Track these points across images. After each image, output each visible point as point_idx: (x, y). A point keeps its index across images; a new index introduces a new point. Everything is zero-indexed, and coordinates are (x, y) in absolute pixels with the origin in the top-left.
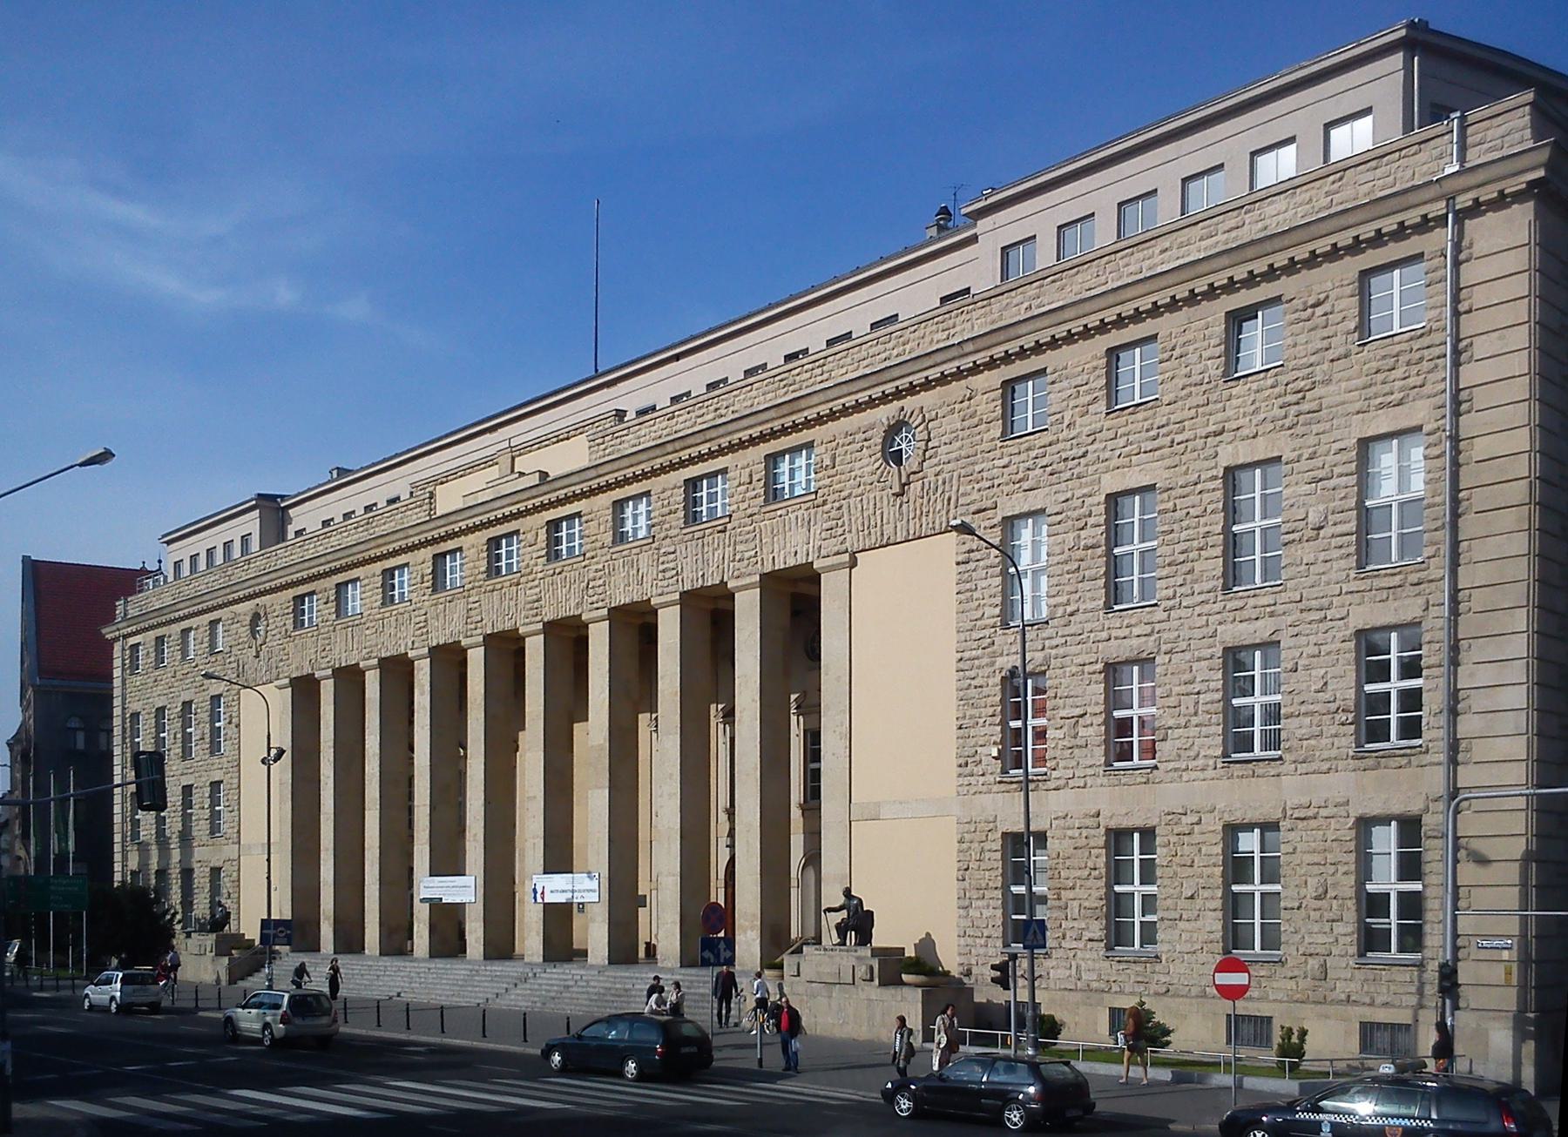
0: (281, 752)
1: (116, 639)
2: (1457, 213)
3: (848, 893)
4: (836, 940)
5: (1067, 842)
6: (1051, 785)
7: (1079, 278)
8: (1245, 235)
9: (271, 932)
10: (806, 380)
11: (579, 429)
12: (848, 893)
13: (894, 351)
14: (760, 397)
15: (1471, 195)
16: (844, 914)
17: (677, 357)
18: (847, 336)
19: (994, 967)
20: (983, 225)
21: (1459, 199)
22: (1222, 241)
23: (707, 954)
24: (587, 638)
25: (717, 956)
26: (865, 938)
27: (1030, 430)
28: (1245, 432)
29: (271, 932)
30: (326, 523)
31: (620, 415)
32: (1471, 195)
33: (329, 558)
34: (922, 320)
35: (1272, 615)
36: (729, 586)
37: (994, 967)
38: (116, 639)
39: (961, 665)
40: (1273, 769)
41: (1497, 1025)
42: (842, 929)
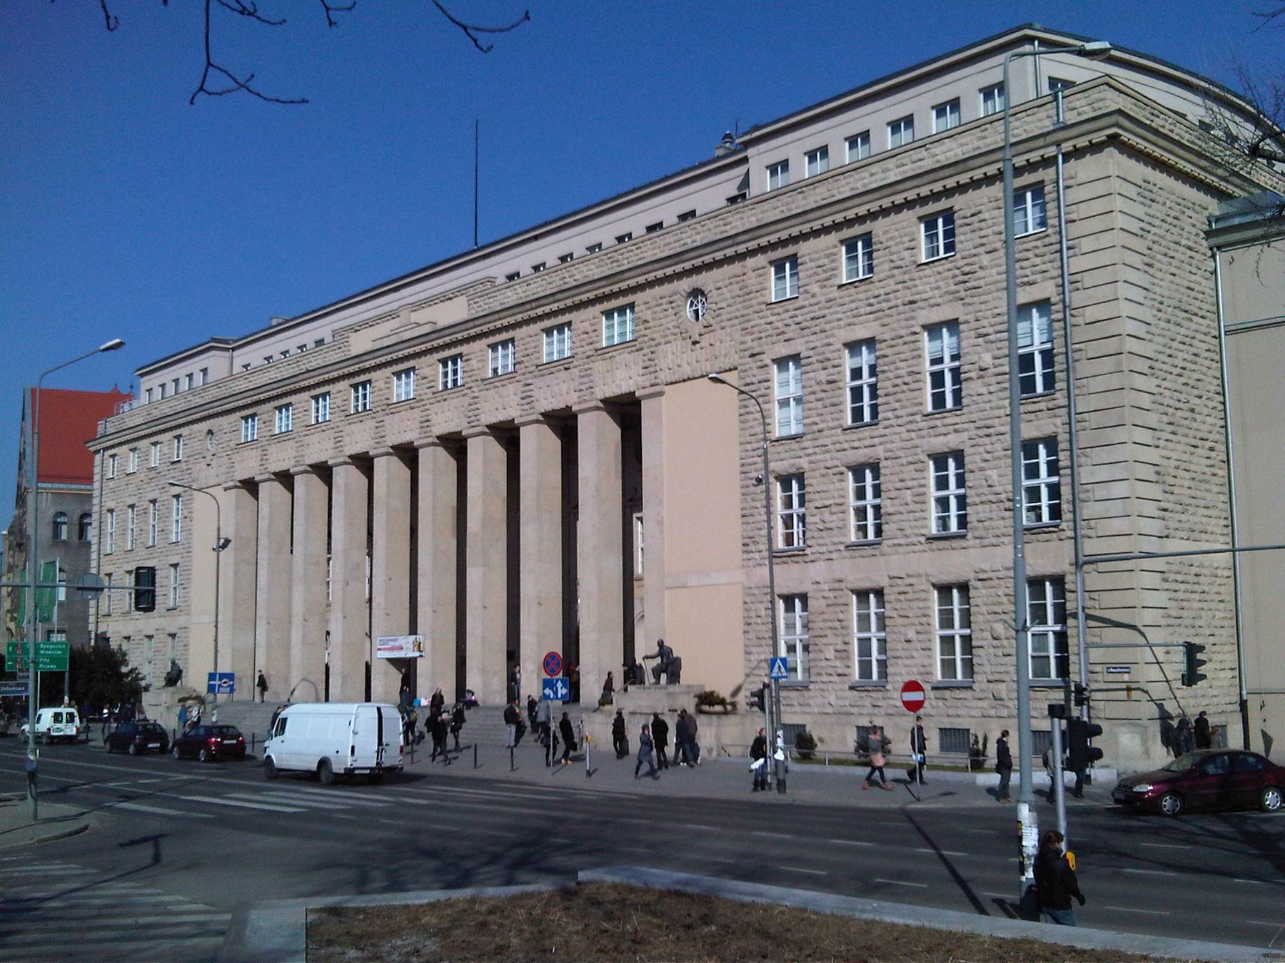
0: (227, 542)
1: (97, 452)
2: (1064, 155)
3: (661, 644)
4: (653, 680)
5: (824, 602)
6: (807, 559)
7: (818, 191)
8: (928, 164)
9: (217, 683)
10: (630, 257)
11: (461, 290)
12: (661, 644)
13: (694, 236)
14: (594, 270)
15: (1071, 143)
16: (658, 660)
17: (536, 238)
18: (660, 225)
19: (1204, 677)
20: (750, 152)
21: (1063, 145)
22: (910, 170)
23: (548, 691)
24: (466, 448)
25: (556, 693)
26: (674, 677)
27: (788, 296)
28: (932, 301)
29: (217, 683)
30: (268, 359)
31: (491, 280)
32: (95, 540)
33: (275, 386)
34: (713, 215)
35: (955, 431)
36: (574, 409)
37: (1204, 677)
38: (97, 452)
39: (744, 469)
40: (962, 543)
41: (1124, 729)
42: (657, 673)
